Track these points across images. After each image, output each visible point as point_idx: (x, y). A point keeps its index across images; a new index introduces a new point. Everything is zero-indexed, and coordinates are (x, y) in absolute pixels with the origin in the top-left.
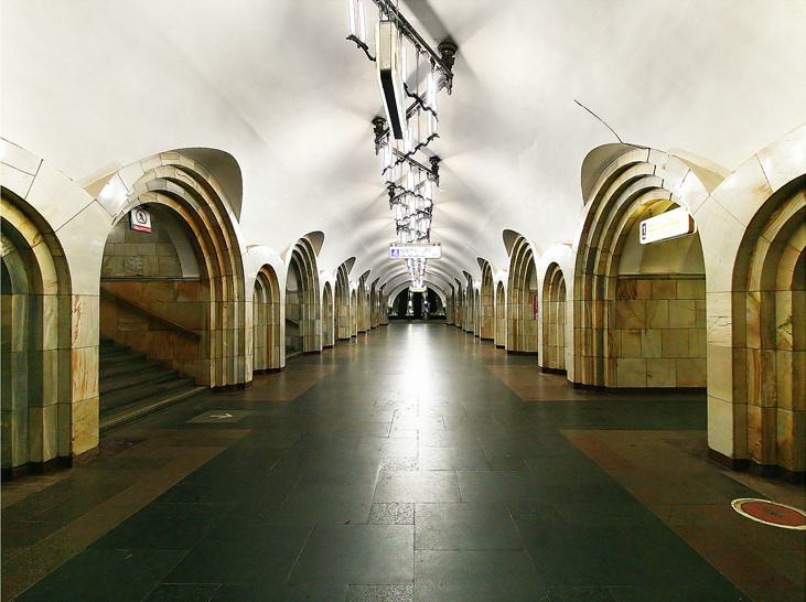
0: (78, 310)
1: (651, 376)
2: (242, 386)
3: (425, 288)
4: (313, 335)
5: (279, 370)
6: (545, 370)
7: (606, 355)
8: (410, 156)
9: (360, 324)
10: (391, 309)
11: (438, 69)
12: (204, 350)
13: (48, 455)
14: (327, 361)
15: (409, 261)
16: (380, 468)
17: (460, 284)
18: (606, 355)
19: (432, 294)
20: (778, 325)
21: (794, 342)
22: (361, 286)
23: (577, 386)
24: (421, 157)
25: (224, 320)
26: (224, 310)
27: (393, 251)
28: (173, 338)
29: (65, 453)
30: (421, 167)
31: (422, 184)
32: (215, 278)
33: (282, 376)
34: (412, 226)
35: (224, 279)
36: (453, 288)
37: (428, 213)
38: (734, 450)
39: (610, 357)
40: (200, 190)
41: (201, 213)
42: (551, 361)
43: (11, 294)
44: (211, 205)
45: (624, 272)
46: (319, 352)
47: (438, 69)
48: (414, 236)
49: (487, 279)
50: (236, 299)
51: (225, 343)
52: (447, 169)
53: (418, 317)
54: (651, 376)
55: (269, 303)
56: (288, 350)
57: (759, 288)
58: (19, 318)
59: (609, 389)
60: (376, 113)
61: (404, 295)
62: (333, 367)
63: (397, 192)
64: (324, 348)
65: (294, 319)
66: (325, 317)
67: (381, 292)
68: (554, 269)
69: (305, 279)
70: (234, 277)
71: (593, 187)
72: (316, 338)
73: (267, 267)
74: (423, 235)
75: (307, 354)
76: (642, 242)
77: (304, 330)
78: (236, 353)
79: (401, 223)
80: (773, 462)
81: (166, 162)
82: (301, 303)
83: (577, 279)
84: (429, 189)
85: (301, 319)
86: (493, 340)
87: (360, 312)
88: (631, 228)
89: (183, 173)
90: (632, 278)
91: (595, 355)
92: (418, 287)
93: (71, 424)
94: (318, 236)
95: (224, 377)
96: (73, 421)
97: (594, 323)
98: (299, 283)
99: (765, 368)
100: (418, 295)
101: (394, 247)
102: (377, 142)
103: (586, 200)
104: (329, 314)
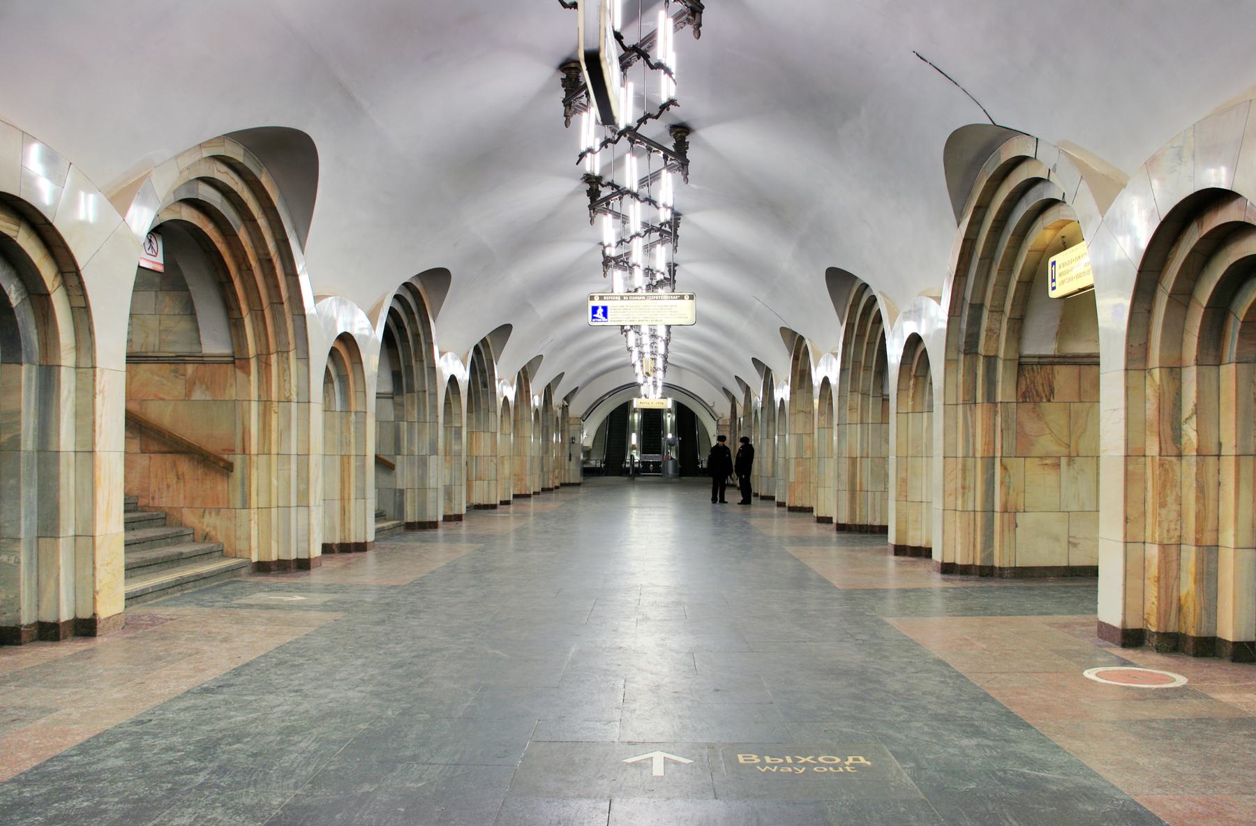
0: (102, 392)
1: (1075, 545)
3: (668, 403)
6: (900, 550)
9: (519, 478)
10: (587, 453)
12: (239, 490)
13: (65, 615)
15: (632, 335)
17: (747, 390)
19: (686, 417)
20: (1183, 419)
21: (1199, 441)
23: (948, 569)
24: (653, 130)
26: (274, 417)
27: (595, 309)
28: (185, 466)
29: (85, 614)
30: (652, 145)
32: (258, 356)
34: (637, 256)
35: (274, 358)
36: (733, 400)
37: (669, 231)
38: (1124, 614)
39: (1005, 510)
42: (911, 533)
43: (21, 364)
44: (262, 222)
45: (436, 456)
48: (639, 279)
49: (801, 376)
51: (274, 481)
52: (706, 147)
53: (648, 474)
54: (1075, 545)
57: (1157, 364)
58: (29, 403)
60: (565, 53)
61: (618, 421)
63: (605, 192)
65: (387, 455)
67: (565, 409)
69: (409, 368)
71: (969, 194)
74: (659, 277)
75: (411, 527)
76: (1053, 294)
79: (612, 252)
80: (1172, 628)
81: (206, 153)
84: (667, 188)
85: (398, 451)
87: (518, 451)
88: (88, 314)
89: (224, 168)
91: (978, 508)
92: (651, 397)
93: (94, 568)
94: (438, 278)
95: (274, 545)
96: (98, 565)
99: (1164, 486)
100: (652, 418)
102: (567, 103)
103: (959, 216)
104: (456, 448)
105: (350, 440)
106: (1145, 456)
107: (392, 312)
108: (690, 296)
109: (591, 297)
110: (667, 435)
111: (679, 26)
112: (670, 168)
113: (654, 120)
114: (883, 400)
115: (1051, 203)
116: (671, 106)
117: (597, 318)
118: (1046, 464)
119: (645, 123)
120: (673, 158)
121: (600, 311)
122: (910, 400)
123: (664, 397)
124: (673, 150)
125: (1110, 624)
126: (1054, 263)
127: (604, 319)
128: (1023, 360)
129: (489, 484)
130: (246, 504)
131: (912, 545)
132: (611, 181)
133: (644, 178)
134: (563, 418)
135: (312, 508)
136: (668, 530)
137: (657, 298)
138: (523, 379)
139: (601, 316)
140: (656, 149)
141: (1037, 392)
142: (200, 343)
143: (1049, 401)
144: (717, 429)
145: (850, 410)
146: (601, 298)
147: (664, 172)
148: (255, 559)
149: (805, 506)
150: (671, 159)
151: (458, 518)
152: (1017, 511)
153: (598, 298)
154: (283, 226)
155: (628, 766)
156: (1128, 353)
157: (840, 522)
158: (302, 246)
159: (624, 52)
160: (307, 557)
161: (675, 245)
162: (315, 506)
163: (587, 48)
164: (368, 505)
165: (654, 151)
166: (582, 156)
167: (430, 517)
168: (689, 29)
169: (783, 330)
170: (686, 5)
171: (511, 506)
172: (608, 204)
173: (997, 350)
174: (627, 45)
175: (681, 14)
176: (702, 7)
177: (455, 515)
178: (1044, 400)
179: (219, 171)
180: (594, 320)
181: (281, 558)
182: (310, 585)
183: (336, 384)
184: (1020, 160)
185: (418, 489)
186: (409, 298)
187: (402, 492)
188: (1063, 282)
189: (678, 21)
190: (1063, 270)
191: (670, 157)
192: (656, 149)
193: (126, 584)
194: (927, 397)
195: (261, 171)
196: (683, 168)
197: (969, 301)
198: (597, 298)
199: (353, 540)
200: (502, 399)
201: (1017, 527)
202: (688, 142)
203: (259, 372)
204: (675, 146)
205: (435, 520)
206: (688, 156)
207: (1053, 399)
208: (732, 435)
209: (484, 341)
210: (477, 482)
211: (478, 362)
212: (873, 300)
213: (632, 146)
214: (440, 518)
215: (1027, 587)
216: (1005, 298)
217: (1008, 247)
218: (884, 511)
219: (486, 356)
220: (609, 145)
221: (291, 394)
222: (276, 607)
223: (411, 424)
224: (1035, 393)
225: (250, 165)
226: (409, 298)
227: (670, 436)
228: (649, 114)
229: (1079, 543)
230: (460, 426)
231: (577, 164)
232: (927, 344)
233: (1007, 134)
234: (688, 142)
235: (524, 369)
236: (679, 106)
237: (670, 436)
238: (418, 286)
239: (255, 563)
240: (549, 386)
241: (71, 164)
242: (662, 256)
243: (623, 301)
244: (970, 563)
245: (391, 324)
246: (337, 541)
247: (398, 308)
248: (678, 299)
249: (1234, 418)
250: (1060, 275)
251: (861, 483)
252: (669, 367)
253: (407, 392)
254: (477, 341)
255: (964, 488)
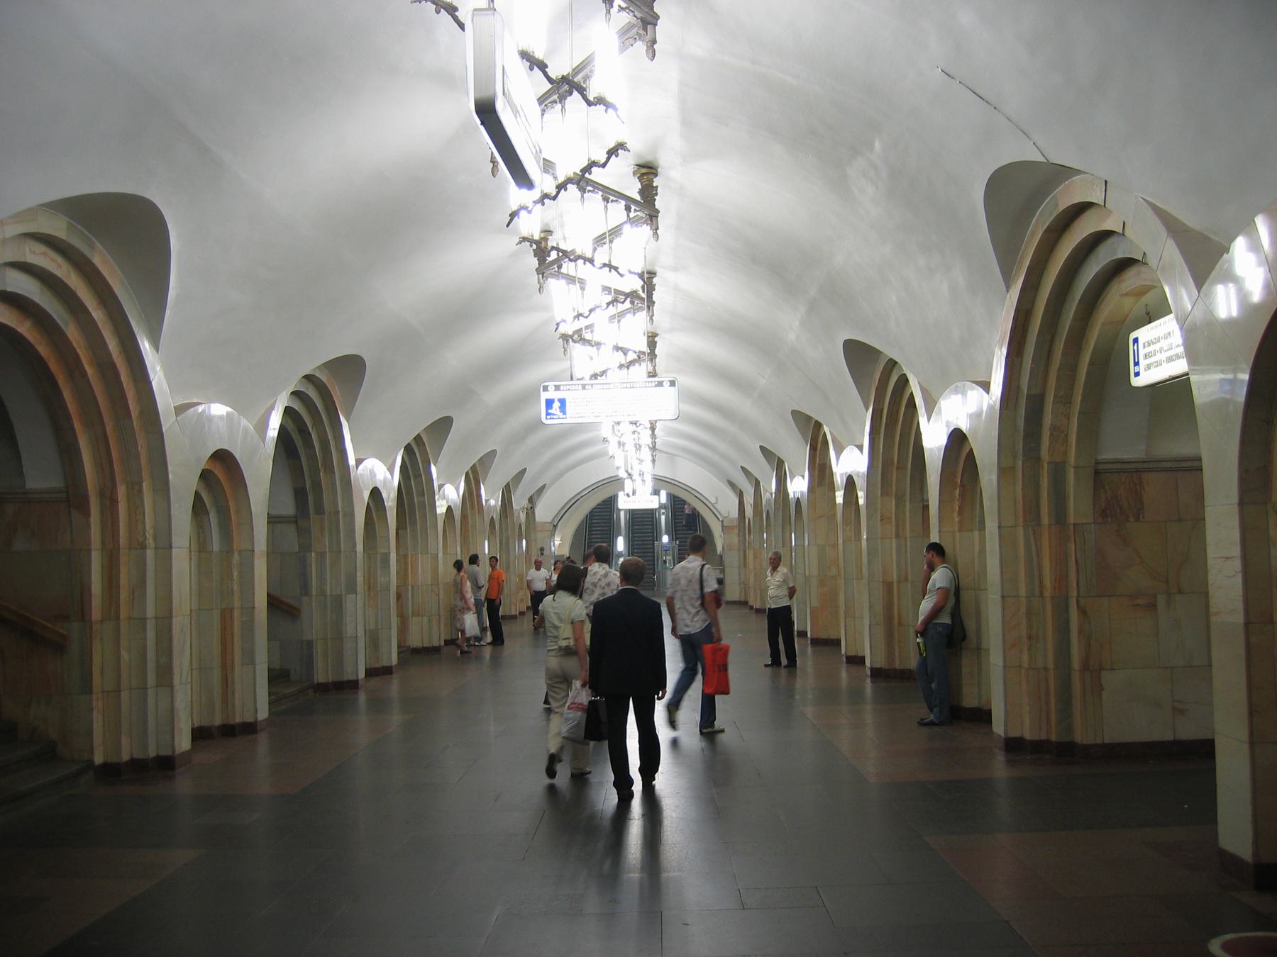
1: (1182, 712)
2: (166, 764)
3: (663, 497)
4: (339, 637)
5: (249, 728)
7: (1076, 664)
8: (597, 175)
11: (621, 9)
14: (379, 705)
16: (360, 480)
17: (757, 484)
18: (1076, 664)
22: (471, 496)
23: (1014, 746)
25: (124, 595)
27: (549, 403)
30: (609, 194)
31: (615, 232)
32: (102, 494)
33: (263, 741)
36: (741, 495)
39: (1085, 667)
40: (74, 281)
41: (72, 332)
44: (97, 314)
45: (354, 595)
46: (354, 685)
47: (621, 9)
50: (150, 541)
55: (228, 550)
56: (277, 677)
59: (1086, 747)
62: (396, 719)
64: (371, 673)
66: (371, 586)
67: (530, 511)
68: (850, 482)
69: (317, 485)
70: (145, 486)
72: (348, 645)
73: (223, 457)
75: (323, 688)
77: (314, 624)
78: (151, 679)
79: (568, 328)
82: (305, 548)
83: (1004, 472)
85: (305, 589)
86: (837, 643)
89: (41, 248)
90: (1137, 471)
95: (125, 741)
97: (1048, 582)
98: (300, 495)
100: (642, 522)
101: (551, 394)
103: (1008, 280)
104: (381, 579)
105: (232, 589)
106: (1018, 596)
107: (288, 411)
108: (670, 381)
109: (674, 381)
110: (661, 538)
111: (627, 43)
112: (633, 222)
113: (601, 168)
114: (923, 507)
115: (1125, 264)
116: (620, 151)
117: (553, 414)
118: (1137, 605)
119: (566, 190)
120: (638, 209)
121: (556, 405)
122: (955, 514)
123: (656, 492)
124: (638, 198)
125: (52, 200)
126: (1136, 340)
127: (561, 415)
128: (1100, 467)
129: (429, 621)
130: (87, 688)
131: (968, 706)
132: (607, 263)
133: (600, 236)
134: (527, 527)
135: (177, 688)
136: (666, 875)
137: (628, 386)
138: (473, 480)
139: (558, 412)
140: (615, 199)
141: (1121, 508)
142: (21, 474)
143: (1137, 520)
144: (723, 530)
145: (881, 520)
146: (557, 388)
147: (627, 227)
148: (98, 759)
149: (832, 637)
150: (635, 210)
151: (387, 671)
152: (1101, 668)
153: (553, 388)
154: (123, 309)
155: (585, 315)
156: (1242, 480)
157: (875, 666)
158: (791, 480)
159: (550, 86)
160: (170, 753)
161: (653, 364)
162: (181, 683)
163: (478, 96)
164: (258, 672)
165: (612, 201)
166: (513, 215)
167: (348, 675)
168: (640, 47)
169: (795, 414)
170: (635, 16)
171: (394, 675)
172: (560, 267)
173: (1066, 453)
174: (554, 77)
175: (630, 27)
176: (657, 17)
177: (383, 667)
178: (1132, 519)
179: (34, 253)
180: (549, 417)
181: (135, 756)
182: (677, 574)
183: (213, 517)
184: (1082, 208)
185: (910, 537)
186: (312, 393)
187: (310, 644)
188: (1149, 367)
189: (627, 37)
190: (1148, 350)
191: (633, 207)
192: (615, 199)
193: (626, 511)
194: (978, 511)
195: (92, 247)
196: (651, 220)
197: (869, 666)
198: (551, 388)
199: (238, 720)
200: (909, 394)
201: (1102, 690)
202: (657, 187)
203: (102, 512)
204: (641, 192)
205: (355, 678)
206: (658, 204)
207: (1144, 517)
208: (741, 538)
209: (418, 439)
210: (414, 618)
211: (412, 466)
212: (904, 381)
213: (582, 196)
214: (362, 675)
215: (519, 536)
216: (1072, 386)
217: (1074, 319)
218: (839, 632)
219: (421, 458)
220: (580, 318)
221: (145, 539)
222: (475, 582)
223: (322, 555)
224: (1118, 511)
225: (76, 242)
226: (312, 393)
227: (665, 539)
228: (554, 200)
229: (584, 66)
230: (387, 551)
231: (508, 226)
232: (976, 445)
233: (1061, 173)
234: (657, 187)
235: (474, 468)
236: (629, 151)
237: (665, 539)
238: (324, 378)
239: (100, 766)
240: (508, 486)
241: (816, 887)
242: (633, 330)
243: (1140, 362)
244: (1043, 737)
245: (291, 427)
246: (218, 721)
247: (297, 406)
248: (656, 386)
249: (1149, 293)
250: (1146, 356)
251: (899, 614)
252: (658, 455)
253: (543, 391)
254: (409, 439)
255: (1030, 638)
